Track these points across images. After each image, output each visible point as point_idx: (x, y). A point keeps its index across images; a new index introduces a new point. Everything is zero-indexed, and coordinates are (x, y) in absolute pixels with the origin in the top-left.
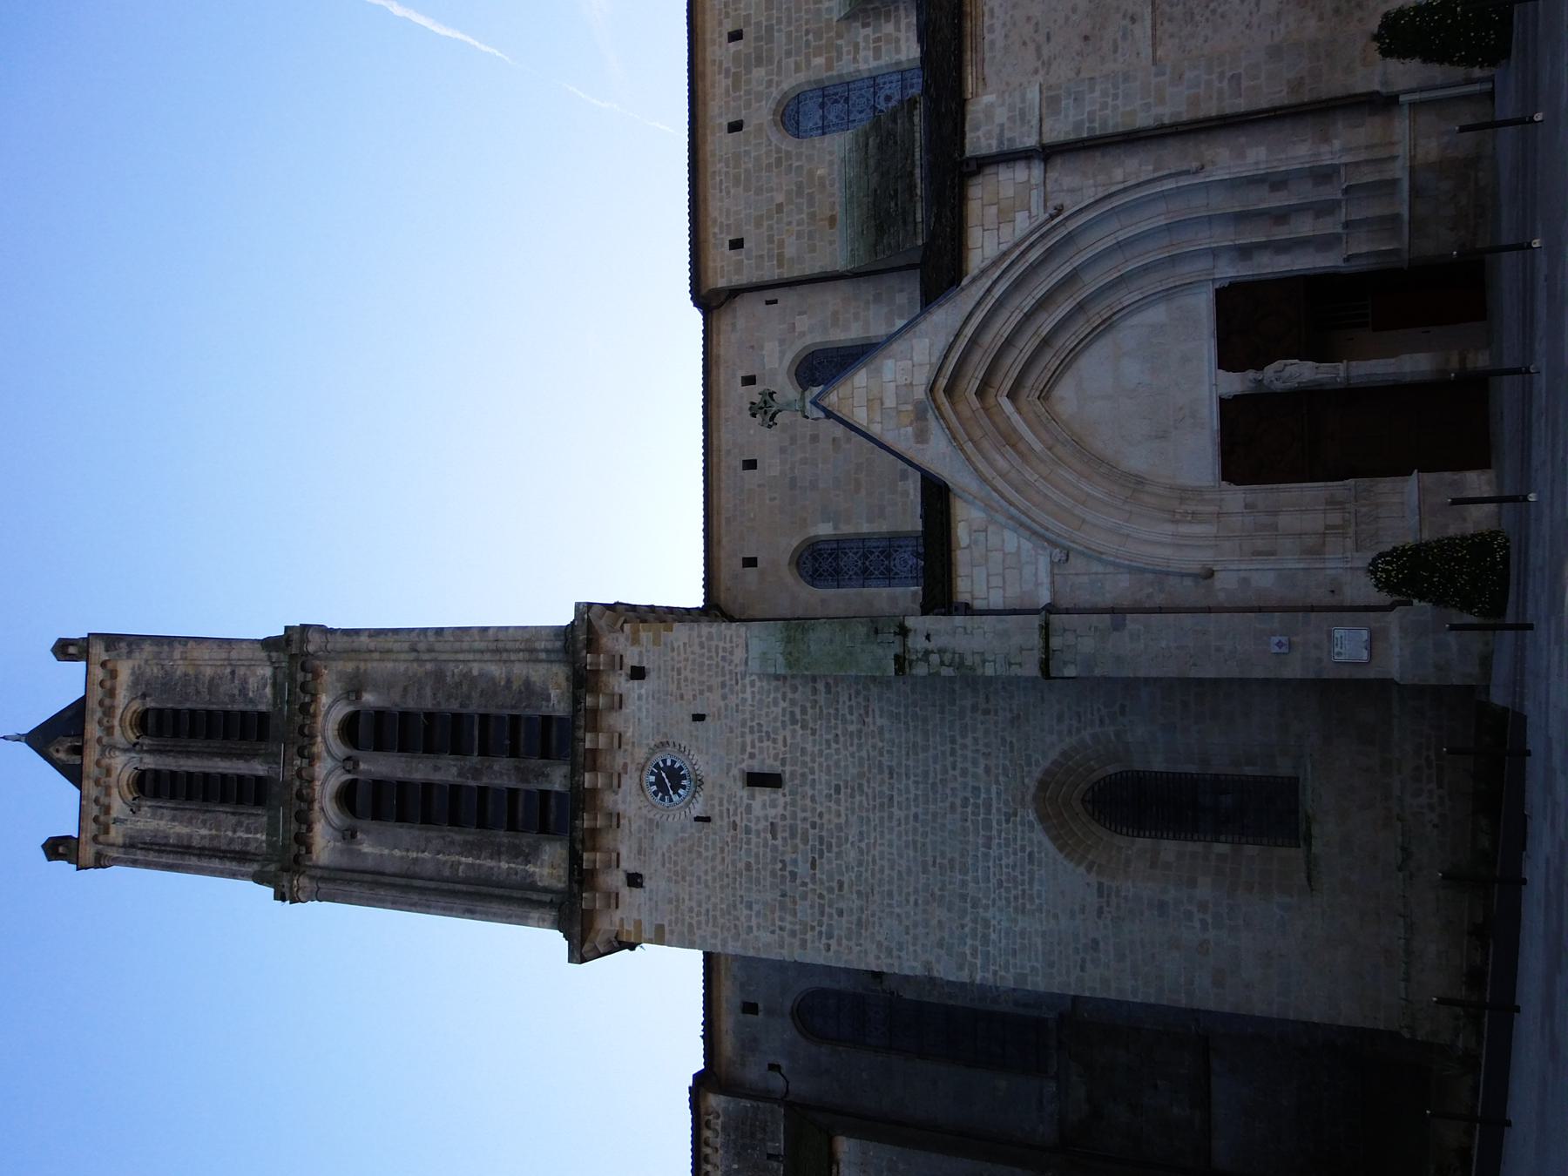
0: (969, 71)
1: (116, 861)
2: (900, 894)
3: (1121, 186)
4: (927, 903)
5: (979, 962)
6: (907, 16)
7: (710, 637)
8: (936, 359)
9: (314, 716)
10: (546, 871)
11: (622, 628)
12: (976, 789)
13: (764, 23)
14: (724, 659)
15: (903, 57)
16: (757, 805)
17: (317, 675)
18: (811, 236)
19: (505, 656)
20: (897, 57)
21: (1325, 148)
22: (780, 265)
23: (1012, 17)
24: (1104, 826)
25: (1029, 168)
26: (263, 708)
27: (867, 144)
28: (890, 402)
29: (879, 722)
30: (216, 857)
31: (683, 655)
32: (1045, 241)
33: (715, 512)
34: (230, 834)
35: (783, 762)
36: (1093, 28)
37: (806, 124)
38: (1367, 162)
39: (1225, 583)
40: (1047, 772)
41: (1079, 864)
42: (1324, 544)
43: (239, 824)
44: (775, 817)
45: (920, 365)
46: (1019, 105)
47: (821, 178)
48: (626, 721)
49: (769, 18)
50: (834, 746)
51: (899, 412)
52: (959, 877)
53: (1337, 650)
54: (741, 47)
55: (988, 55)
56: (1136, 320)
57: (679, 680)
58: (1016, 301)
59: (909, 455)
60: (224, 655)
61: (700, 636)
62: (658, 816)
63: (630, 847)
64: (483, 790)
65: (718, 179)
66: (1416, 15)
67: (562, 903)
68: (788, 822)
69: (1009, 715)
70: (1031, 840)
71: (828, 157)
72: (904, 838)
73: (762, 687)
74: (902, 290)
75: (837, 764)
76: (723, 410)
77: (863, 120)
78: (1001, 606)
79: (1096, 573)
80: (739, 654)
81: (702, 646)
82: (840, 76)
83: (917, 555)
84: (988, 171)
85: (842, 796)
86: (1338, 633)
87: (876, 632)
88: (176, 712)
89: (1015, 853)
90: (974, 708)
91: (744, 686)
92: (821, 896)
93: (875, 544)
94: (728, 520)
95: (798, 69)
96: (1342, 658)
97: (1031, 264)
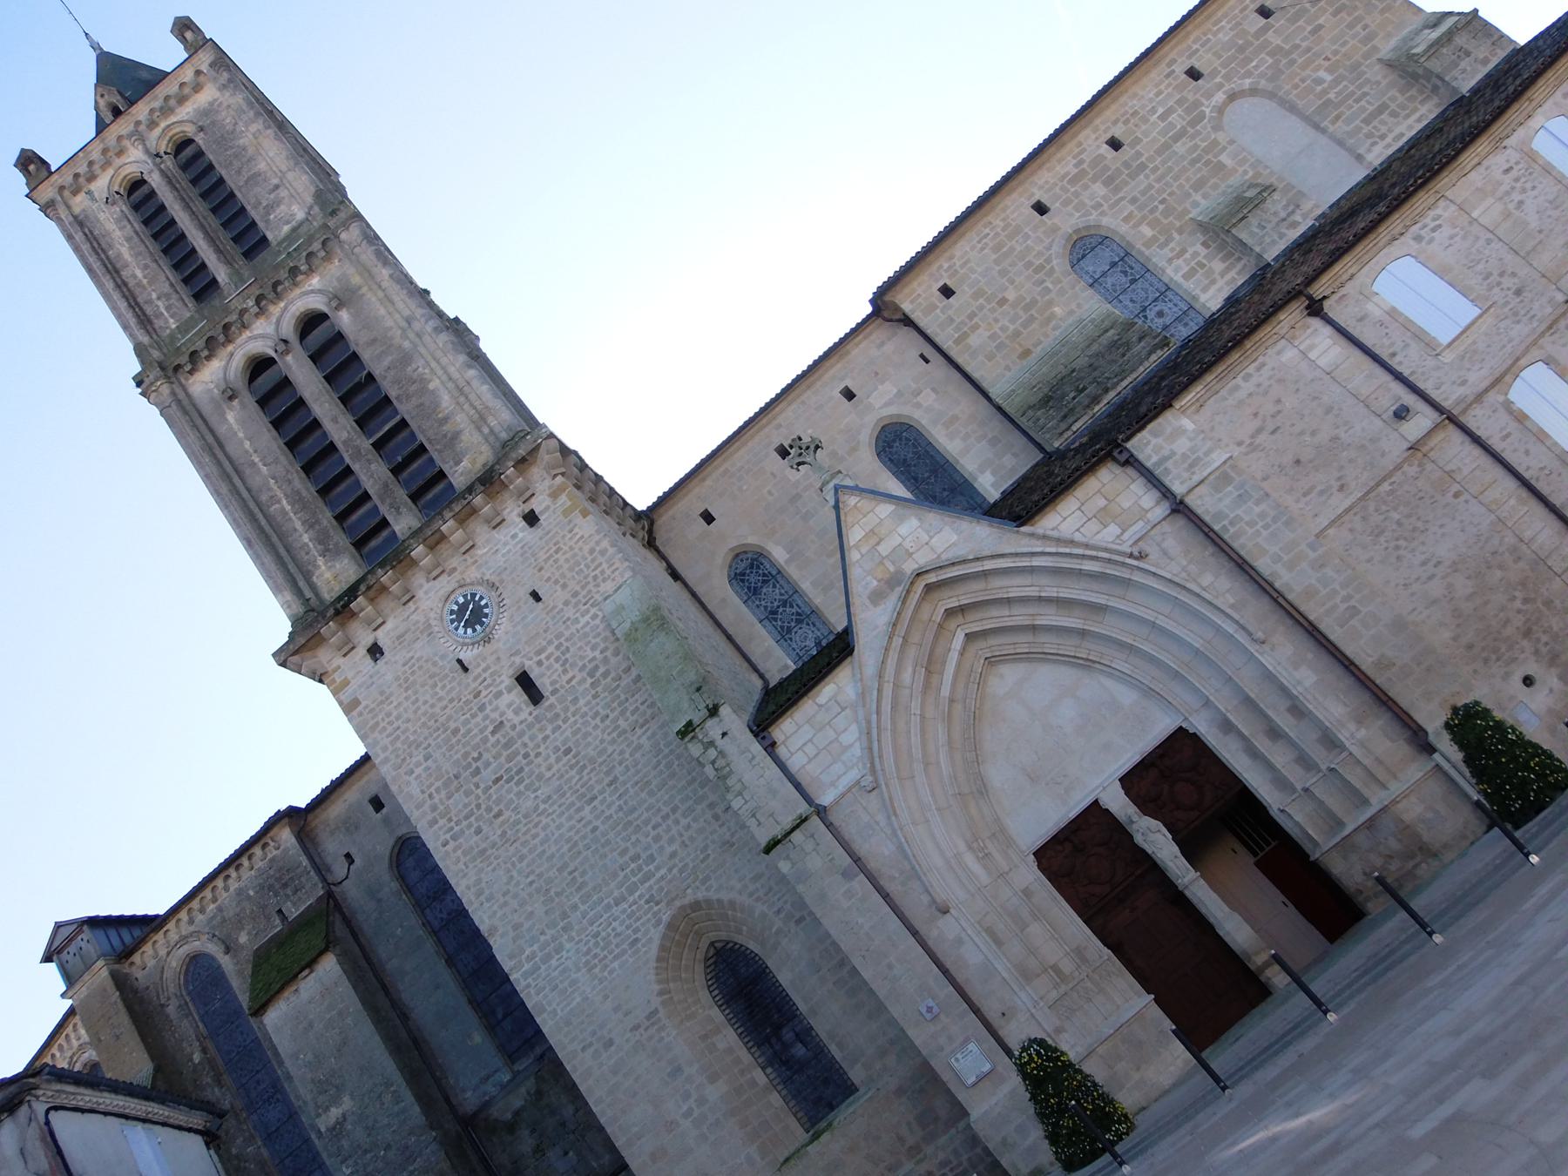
0: (1198, 389)
1: (59, 221)
2: (528, 866)
3: (1197, 590)
4: (538, 891)
5: (527, 967)
6: (1238, 273)
7: (603, 552)
9: (296, 284)
10: (328, 575)
11: (555, 476)
12: (652, 858)
13: (1143, 159)
14: (595, 578)
15: (1203, 298)
16: (507, 698)
17: (328, 258)
18: (999, 347)
19: (462, 399)
21: (1352, 726)
22: (958, 342)
23: (1270, 386)
24: (707, 974)
26: (270, 236)
27: (1106, 331)
28: (884, 549)
29: (644, 740)
30: (127, 300)
31: (572, 543)
34: (154, 296)
35: (554, 692)
36: (1311, 461)
37: (1089, 265)
38: (1365, 768)
39: (943, 931)
40: (708, 902)
41: (659, 982)
42: (1038, 975)
43: (167, 296)
44: (509, 721)
46: (1200, 454)
47: (1053, 316)
48: (488, 541)
49: (1151, 159)
50: (598, 720)
51: (881, 563)
52: (576, 899)
53: (959, 1056)
54: (1109, 157)
55: (1223, 392)
56: (1109, 683)
57: (551, 556)
58: (1044, 580)
59: (855, 600)
60: (284, 168)
61: (598, 543)
62: (436, 629)
63: (397, 627)
64: (348, 471)
65: (987, 231)
66: (1491, 728)
67: (313, 610)
68: (513, 734)
69: (727, 836)
70: (647, 931)
71: (1073, 306)
72: (572, 833)
74: (1015, 455)
75: (587, 734)
76: (809, 392)
79: (877, 823)
80: (608, 587)
81: (592, 551)
82: (1148, 259)
83: (818, 644)
84: (1130, 471)
85: (565, 759)
86: (972, 1046)
87: (698, 689)
88: (211, 167)
89: (628, 928)
90: (712, 806)
91: (587, 611)
92: (478, 806)
94: (726, 471)
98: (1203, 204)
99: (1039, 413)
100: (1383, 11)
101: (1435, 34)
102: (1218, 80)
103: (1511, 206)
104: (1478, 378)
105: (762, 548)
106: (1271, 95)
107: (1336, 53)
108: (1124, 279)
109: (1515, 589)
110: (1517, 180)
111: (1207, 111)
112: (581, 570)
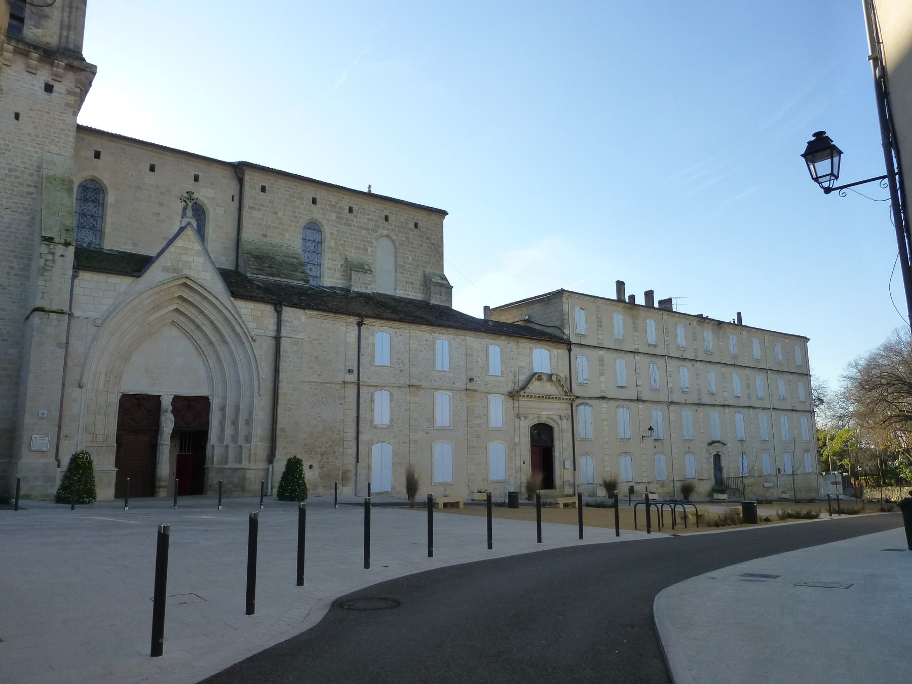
3: (259, 365)
6: (341, 283)
7: (66, 135)
8: (200, 281)
14: (53, 140)
15: (326, 279)
18: (260, 224)
20: (326, 277)
25: (273, 331)
27: (294, 258)
28: (184, 258)
32: (243, 333)
33: (129, 143)
37: (309, 232)
39: (73, 392)
45: (199, 275)
54: (346, 211)
61: (69, 130)
65: (294, 188)
66: (300, 470)
73: (34, 157)
77: (304, 258)
78: (74, 293)
80: (55, 150)
81: (62, 130)
83: (90, 244)
84: (276, 314)
87: (67, 230)
90: (11, 268)
91: (35, 147)
93: (99, 223)
95: (331, 234)
96: (33, 438)
97: (234, 327)
98: (354, 255)
99: (252, 259)
100: (437, 260)
101: (440, 281)
102: (390, 228)
103: (419, 349)
104: (373, 381)
105: (107, 189)
106: (396, 248)
107: (418, 257)
108: (313, 248)
109: (330, 441)
110: (426, 345)
111: (379, 232)
112: (50, 131)
